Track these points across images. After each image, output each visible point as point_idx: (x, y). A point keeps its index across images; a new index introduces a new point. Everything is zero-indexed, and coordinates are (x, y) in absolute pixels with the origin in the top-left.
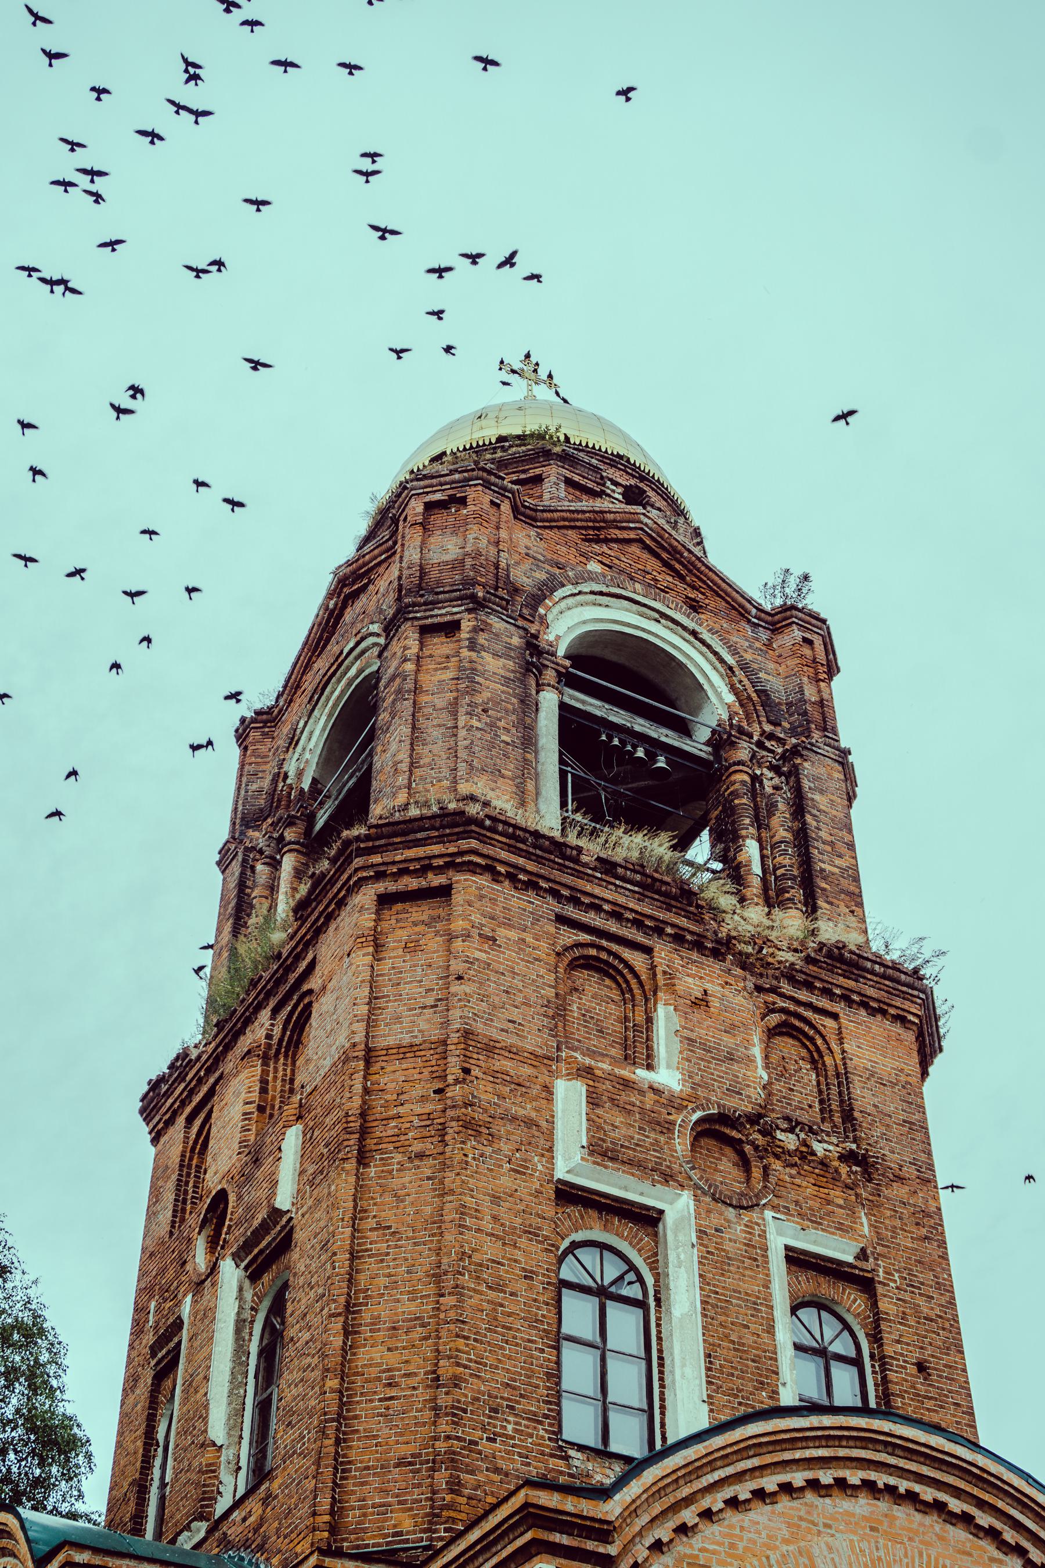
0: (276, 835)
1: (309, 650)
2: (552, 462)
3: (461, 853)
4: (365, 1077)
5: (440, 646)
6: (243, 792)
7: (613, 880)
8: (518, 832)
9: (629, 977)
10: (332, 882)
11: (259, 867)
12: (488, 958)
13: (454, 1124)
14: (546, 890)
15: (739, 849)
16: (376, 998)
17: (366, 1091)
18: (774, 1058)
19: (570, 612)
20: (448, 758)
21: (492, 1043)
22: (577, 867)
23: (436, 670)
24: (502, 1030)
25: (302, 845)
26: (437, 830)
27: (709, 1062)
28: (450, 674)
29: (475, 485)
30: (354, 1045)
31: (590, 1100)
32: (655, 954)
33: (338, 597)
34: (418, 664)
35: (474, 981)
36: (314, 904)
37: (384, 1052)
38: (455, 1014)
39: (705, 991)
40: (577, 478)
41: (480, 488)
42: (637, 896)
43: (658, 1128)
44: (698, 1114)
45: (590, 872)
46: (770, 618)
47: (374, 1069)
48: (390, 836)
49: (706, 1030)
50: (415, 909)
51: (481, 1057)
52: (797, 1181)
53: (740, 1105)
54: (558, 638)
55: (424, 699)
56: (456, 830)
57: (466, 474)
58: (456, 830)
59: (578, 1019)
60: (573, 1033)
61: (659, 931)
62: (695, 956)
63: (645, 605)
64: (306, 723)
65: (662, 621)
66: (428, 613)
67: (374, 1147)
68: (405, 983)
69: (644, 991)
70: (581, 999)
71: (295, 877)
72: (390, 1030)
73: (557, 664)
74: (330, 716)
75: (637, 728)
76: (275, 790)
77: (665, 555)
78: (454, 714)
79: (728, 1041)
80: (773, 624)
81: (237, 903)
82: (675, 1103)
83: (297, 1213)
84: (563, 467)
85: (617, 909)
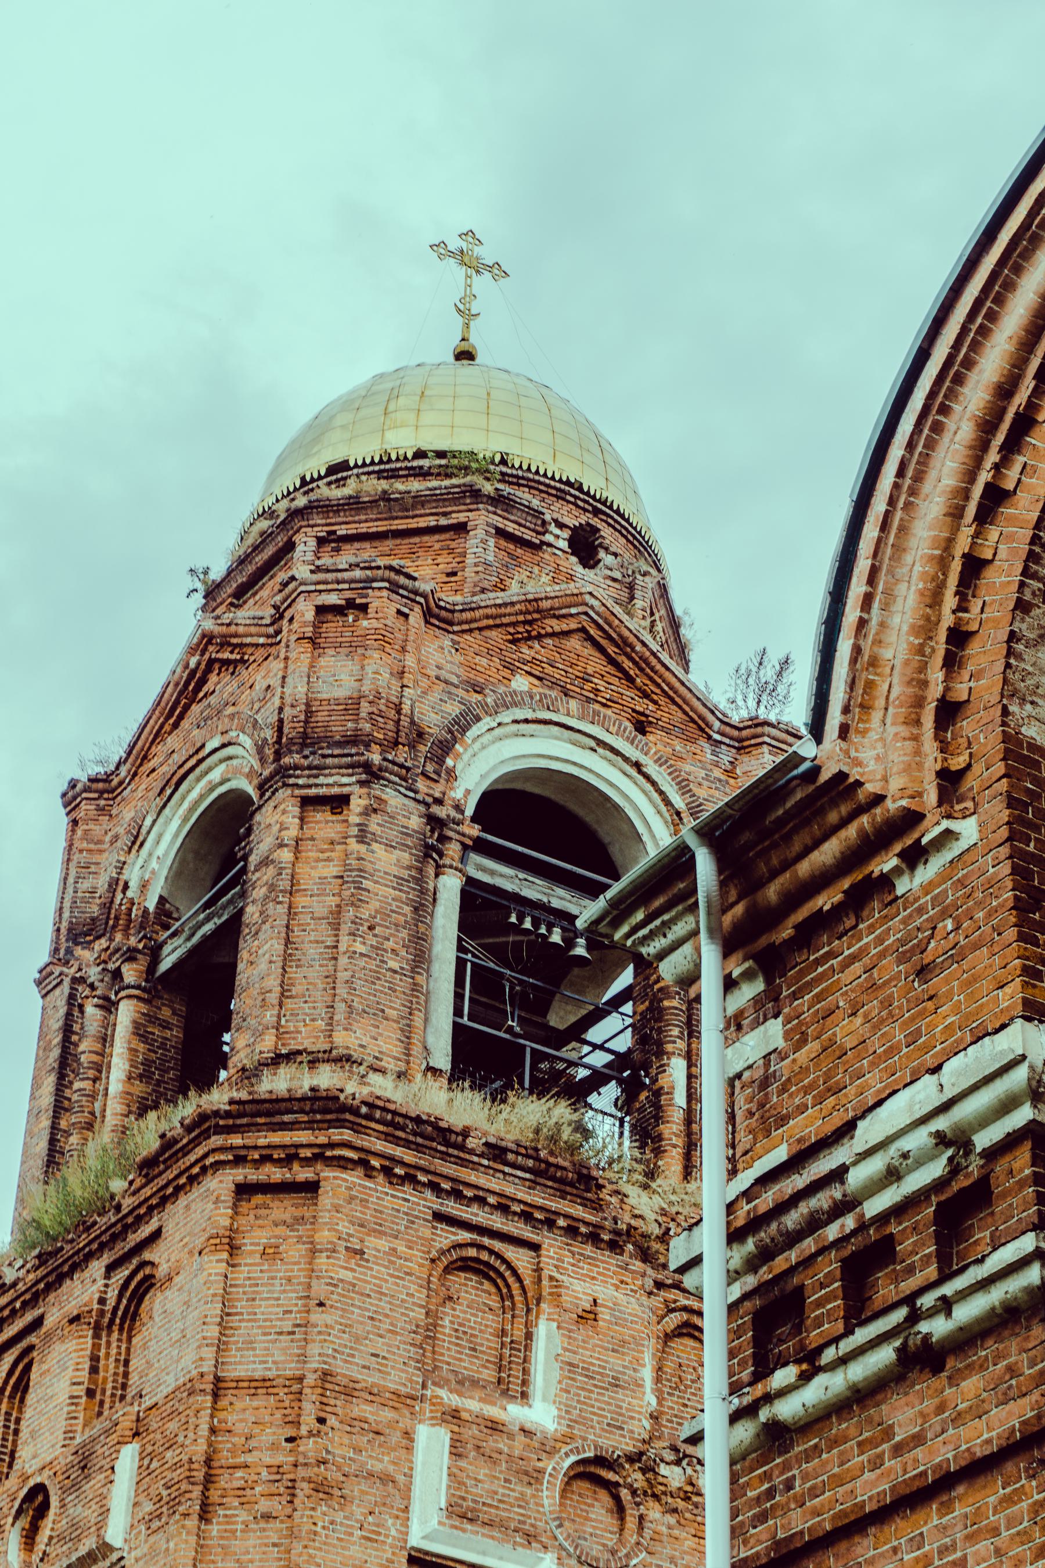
0: (111, 966)
1: (162, 714)
2: (481, 506)
3: (332, 1146)
4: (212, 1416)
5: (324, 825)
6: (70, 890)
7: (501, 1167)
8: (397, 1119)
9: (511, 1280)
10: (185, 1151)
11: (90, 1010)
12: (354, 1278)
13: (305, 1485)
14: (424, 1184)
15: (662, 1069)
16: (228, 1314)
17: (213, 1431)
18: (670, 1366)
19: (485, 752)
20: (325, 989)
21: (351, 1385)
22: (462, 1155)
23: (318, 860)
24: (364, 1367)
25: (144, 990)
26: (307, 1113)
27: (592, 1392)
28: (333, 870)
29: (380, 589)
30: (202, 1375)
31: (454, 1450)
32: (543, 1252)
33: (202, 654)
34: (297, 850)
35: (337, 1308)
36: (162, 1167)
37: (234, 1384)
38: (314, 1350)
39: (595, 1301)
40: (511, 528)
41: (385, 593)
42: (527, 1183)
43: (526, 1479)
44: (573, 1458)
45: (475, 1159)
46: (736, 733)
47: (223, 1403)
48: (254, 1115)
49: (591, 1349)
50: (277, 1203)
51: (338, 1403)
52: (676, 1532)
53: (620, 1443)
54: (468, 792)
55: (301, 901)
56: (329, 1117)
57: (368, 572)
58: (329, 1117)
59: (450, 1336)
60: (443, 1355)
61: (550, 1224)
62: (589, 1249)
63: (579, 731)
64: (154, 821)
65: (600, 750)
66: (312, 781)
67: (218, 1500)
68: (261, 1299)
69: (526, 1298)
70: (454, 1309)
71: (134, 1033)
72: (242, 1356)
73: (464, 835)
74: (185, 820)
75: (556, 903)
76: (112, 902)
77: (611, 650)
78: (336, 927)
79: (615, 1362)
80: (740, 740)
81: (61, 1056)
82: (548, 1448)
83: (129, 1553)
84: (495, 513)
85: (503, 1201)
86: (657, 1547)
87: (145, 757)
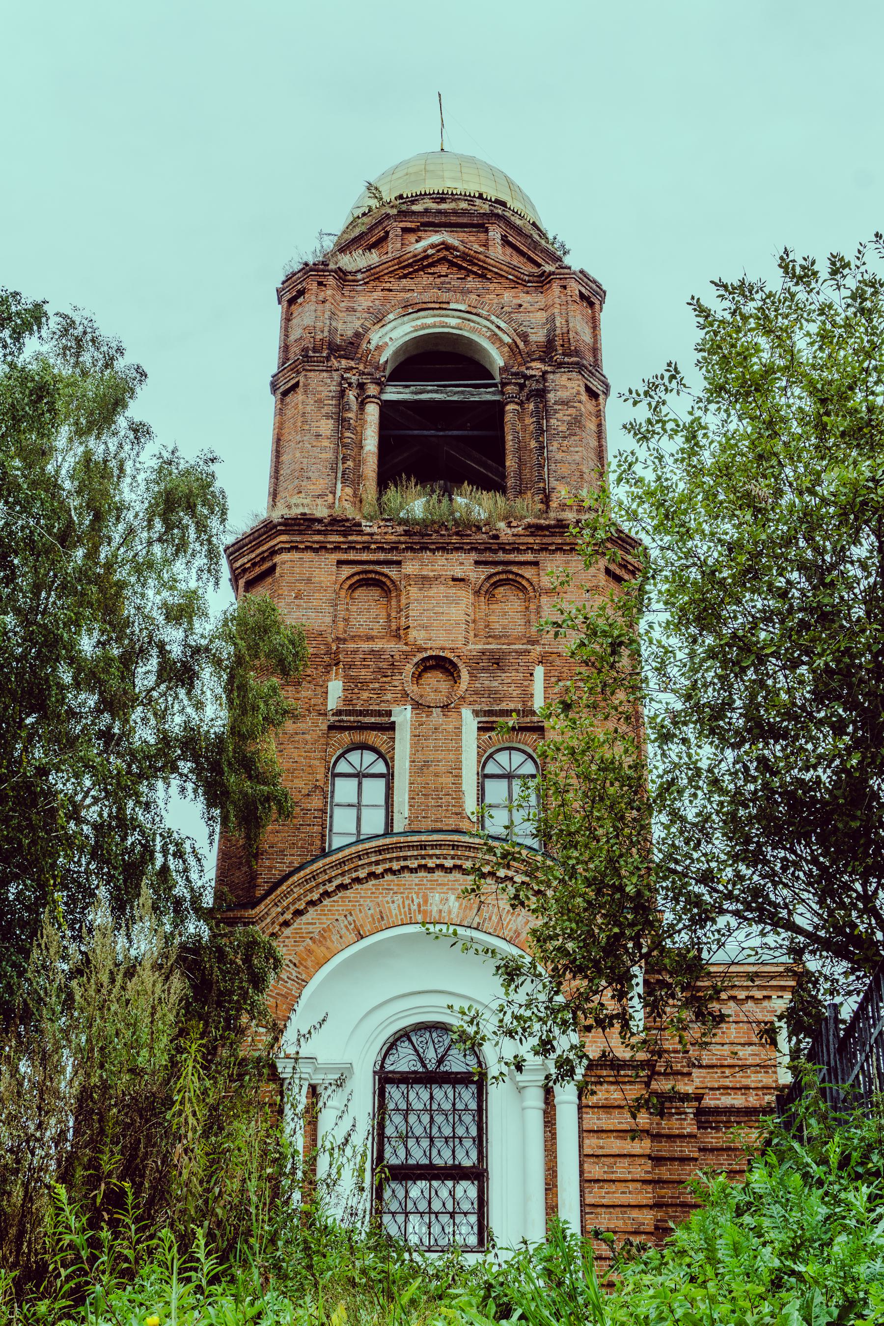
86: (290, 748)
87: (378, 278)
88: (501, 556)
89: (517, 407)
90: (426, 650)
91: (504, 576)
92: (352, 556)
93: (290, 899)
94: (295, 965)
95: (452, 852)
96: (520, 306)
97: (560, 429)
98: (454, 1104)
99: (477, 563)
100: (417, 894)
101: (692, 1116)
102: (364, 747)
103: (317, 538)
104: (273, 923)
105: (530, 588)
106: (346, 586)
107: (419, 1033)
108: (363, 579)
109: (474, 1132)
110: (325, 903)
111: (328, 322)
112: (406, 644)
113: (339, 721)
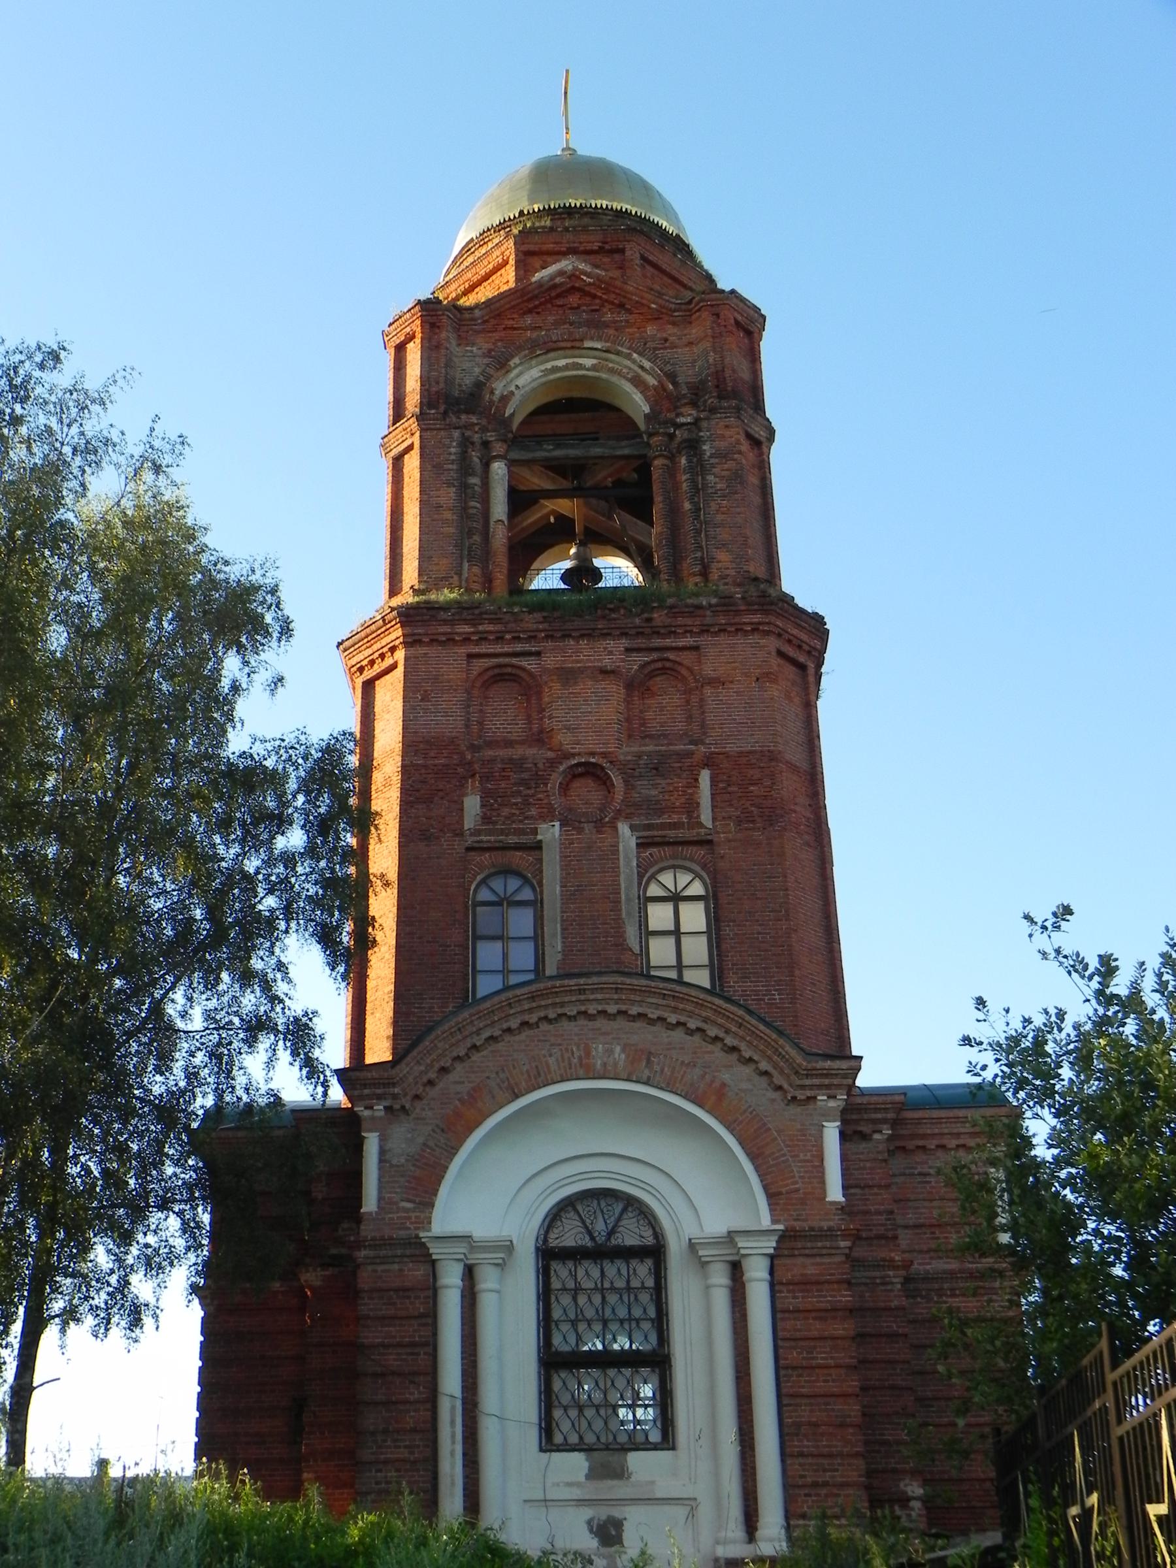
87: (499, 315)
88: (657, 642)
89: (666, 462)
90: (573, 755)
91: (659, 665)
92: (483, 649)
93: (434, 1056)
94: (443, 1130)
95: (616, 996)
96: (666, 340)
97: (719, 486)
98: (628, 1282)
99: (628, 650)
100: (578, 1046)
101: (899, 1286)
102: (507, 871)
103: (442, 629)
104: (416, 1083)
105: (691, 678)
106: (478, 684)
107: (585, 1202)
108: (499, 675)
109: (652, 1313)
110: (474, 1058)
111: (443, 371)
112: (550, 749)
113: (478, 842)
